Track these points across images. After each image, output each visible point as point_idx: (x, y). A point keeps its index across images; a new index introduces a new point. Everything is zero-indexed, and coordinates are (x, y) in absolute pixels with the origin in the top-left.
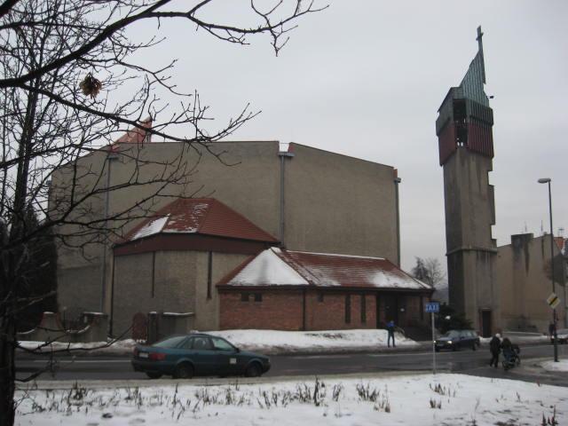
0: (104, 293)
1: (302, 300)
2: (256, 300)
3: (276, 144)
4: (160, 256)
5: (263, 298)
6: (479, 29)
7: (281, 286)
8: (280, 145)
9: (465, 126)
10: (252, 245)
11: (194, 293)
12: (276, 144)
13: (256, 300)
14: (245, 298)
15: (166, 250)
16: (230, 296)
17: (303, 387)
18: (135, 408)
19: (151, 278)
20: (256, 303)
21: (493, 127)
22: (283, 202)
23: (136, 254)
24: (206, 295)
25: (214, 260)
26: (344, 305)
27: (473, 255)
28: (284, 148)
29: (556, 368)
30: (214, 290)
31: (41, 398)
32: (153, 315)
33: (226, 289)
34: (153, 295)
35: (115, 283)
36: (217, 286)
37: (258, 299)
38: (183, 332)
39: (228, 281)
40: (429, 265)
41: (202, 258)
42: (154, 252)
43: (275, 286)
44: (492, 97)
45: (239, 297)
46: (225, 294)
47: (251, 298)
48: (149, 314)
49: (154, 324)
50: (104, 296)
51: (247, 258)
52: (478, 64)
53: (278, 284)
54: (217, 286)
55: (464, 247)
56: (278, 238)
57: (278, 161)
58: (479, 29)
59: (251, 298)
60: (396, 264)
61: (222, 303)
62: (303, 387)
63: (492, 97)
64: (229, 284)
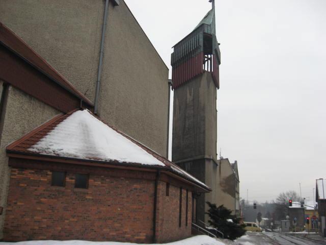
5: (91, 181)
7: (124, 164)
10: (66, 100)
16: (29, 174)
21: (219, 92)
22: (101, 53)
23: (56, 109)
26: (179, 194)
29: (222, 241)
31: (48, 112)
33: (23, 159)
37: (82, 184)
39: (30, 145)
40: (222, 159)
43: (115, 163)
45: (46, 178)
46: (22, 168)
51: (49, 115)
52: (211, 14)
53: (121, 160)
55: (207, 156)
56: (91, 101)
60: (165, 157)
64: (34, 149)
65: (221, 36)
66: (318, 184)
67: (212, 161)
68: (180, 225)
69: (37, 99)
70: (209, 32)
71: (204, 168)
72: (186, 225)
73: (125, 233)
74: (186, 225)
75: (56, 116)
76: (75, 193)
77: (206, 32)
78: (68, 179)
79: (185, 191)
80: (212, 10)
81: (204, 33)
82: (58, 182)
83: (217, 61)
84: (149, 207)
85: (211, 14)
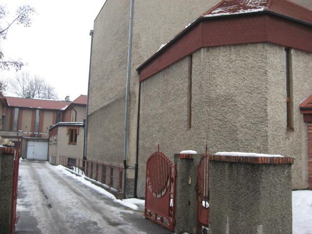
0: (128, 129)
4: (202, 58)
11: (264, 120)
15: (211, 46)
17: (131, 191)
19: (185, 99)
24: (285, 125)
25: (294, 63)
30: (297, 115)
32: (189, 158)
34: (190, 126)
35: (141, 116)
36: (302, 109)
38: (239, 12)
41: (276, 58)
42: (191, 56)
48: (177, 156)
50: (128, 134)
54: (302, 109)
62: (131, 191)
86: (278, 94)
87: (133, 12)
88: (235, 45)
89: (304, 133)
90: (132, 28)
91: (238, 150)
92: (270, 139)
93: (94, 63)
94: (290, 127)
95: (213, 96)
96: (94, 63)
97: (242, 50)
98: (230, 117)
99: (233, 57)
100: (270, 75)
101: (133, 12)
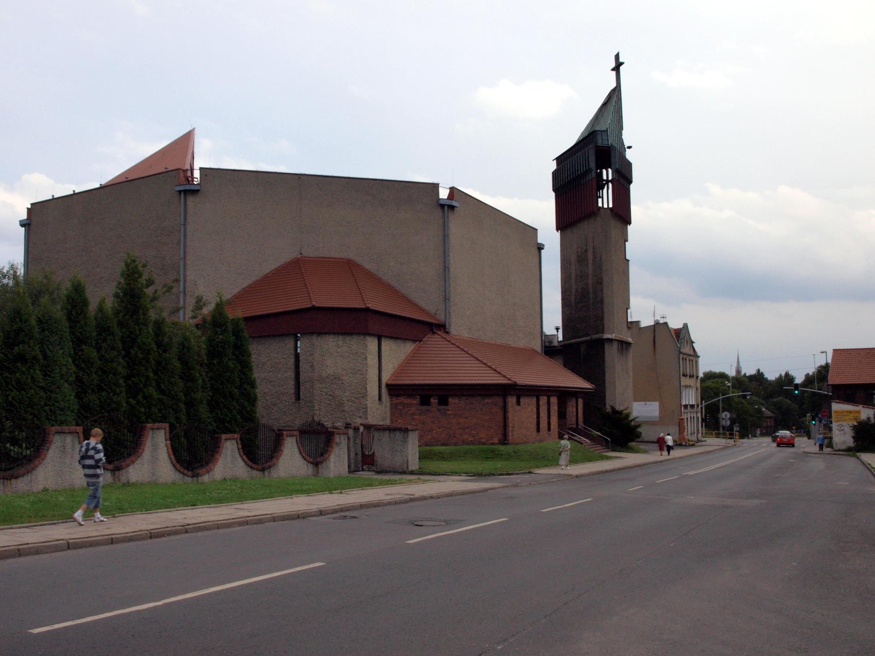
1: (501, 404)
2: (440, 404)
3: (435, 187)
5: (450, 400)
6: (617, 57)
8: (440, 189)
9: (593, 173)
12: (435, 187)
13: (440, 404)
14: (425, 401)
16: (402, 399)
18: (816, 449)
19: (291, 374)
20: (442, 407)
21: (632, 187)
23: (279, 336)
24: (377, 398)
25: (383, 348)
27: (615, 345)
28: (444, 194)
30: (384, 390)
36: (387, 385)
37: (443, 401)
41: (372, 344)
44: (629, 147)
46: (398, 396)
47: (434, 401)
49: (358, 441)
52: (614, 98)
54: (387, 385)
55: (607, 336)
57: (438, 212)
58: (617, 57)
59: (434, 401)
60: (691, 353)
61: (394, 407)
63: (629, 147)
65: (638, 139)
66: (740, 360)
67: (96, 500)
68: (538, 430)
69: (326, 333)
70: (605, 143)
71: (604, 352)
72: (549, 429)
73: (481, 438)
74: (549, 429)
75: (630, 363)
76: (439, 410)
77: (600, 143)
78: (432, 400)
79: (546, 398)
80: (616, 88)
81: (597, 147)
82: (425, 402)
83: (624, 178)
84: (499, 417)
85: (614, 98)
86: (373, 374)
87: (185, 252)
88: (342, 334)
89: (388, 404)
90: (185, 271)
91: (313, 562)
92: (369, 409)
93: (302, 177)
94: (380, 399)
95: (324, 375)
96: (302, 177)
97: (348, 338)
98: (337, 393)
99: (340, 343)
100: (369, 359)
101: (185, 252)
